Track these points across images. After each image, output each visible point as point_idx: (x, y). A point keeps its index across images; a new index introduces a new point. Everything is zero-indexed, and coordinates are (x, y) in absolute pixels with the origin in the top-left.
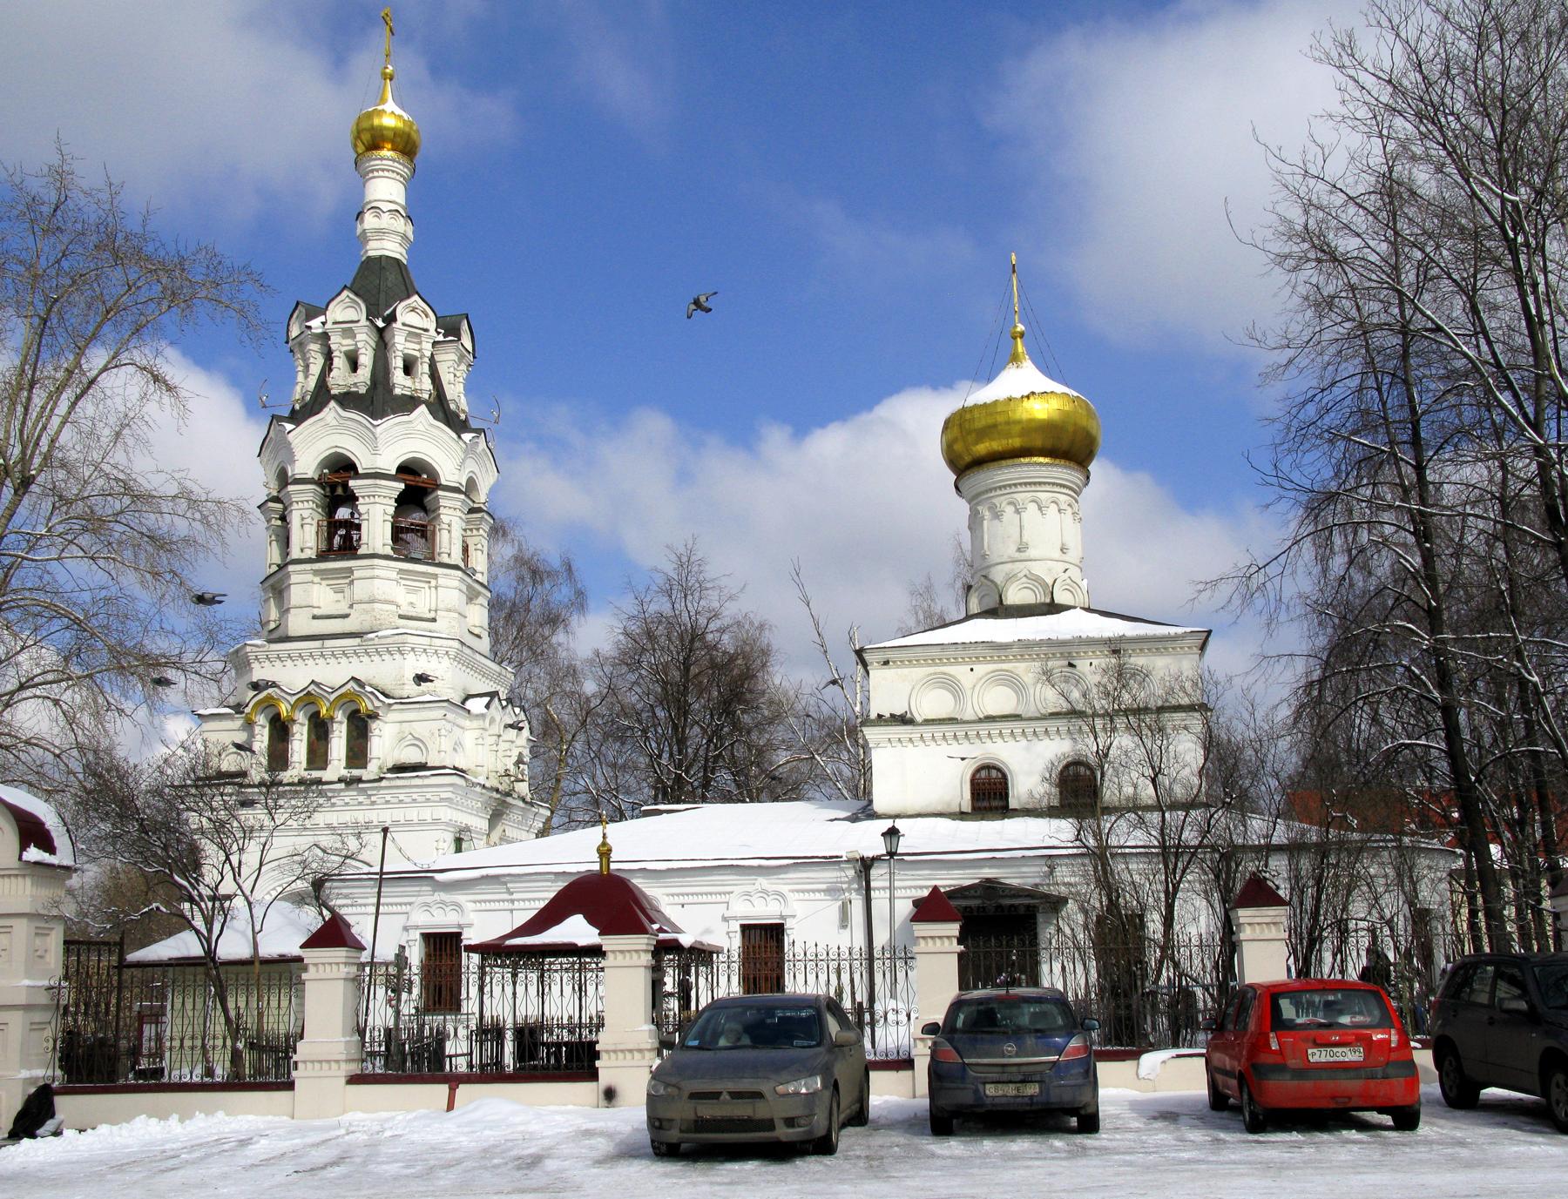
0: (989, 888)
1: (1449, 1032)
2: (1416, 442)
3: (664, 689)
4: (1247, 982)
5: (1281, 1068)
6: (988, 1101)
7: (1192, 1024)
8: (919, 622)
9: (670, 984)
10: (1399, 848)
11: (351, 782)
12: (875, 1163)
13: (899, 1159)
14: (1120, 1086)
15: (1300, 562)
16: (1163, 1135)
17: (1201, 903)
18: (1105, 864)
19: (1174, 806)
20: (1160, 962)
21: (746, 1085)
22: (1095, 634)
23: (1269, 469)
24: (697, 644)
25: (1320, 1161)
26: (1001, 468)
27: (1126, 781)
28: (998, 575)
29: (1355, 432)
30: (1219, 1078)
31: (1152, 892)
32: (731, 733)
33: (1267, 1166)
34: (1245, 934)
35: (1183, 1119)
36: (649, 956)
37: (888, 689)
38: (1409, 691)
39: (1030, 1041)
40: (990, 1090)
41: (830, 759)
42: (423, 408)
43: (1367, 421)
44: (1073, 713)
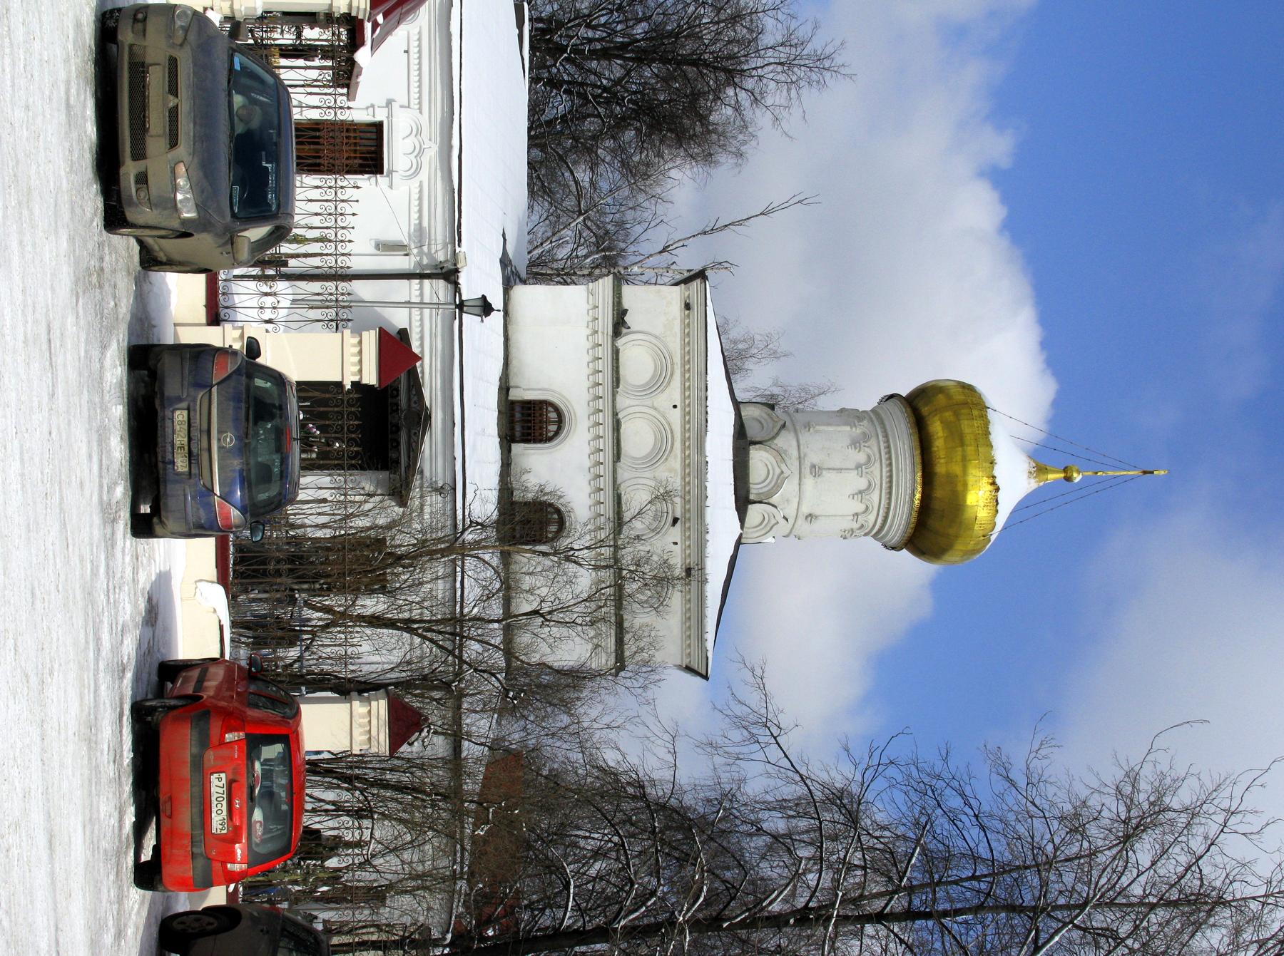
0: (421, 418)
1: (244, 923)
2: (910, 915)
3: (670, 34)
4: (304, 708)
5: (204, 743)
6: (168, 413)
7: (259, 643)
8: (735, 342)
9: (312, 34)
10: (454, 877)
12: (94, 279)
13: (100, 305)
14: (189, 562)
15: (780, 783)
16: (130, 609)
17: (396, 657)
18: (444, 553)
19: (508, 632)
20: (328, 610)
21: (186, 127)
22: (710, 549)
23: (891, 753)
24: (722, 76)
25: (98, 783)
26: (912, 448)
27: (538, 578)
28: (785, 441)
29: (923, 850)
30: (195, 673)
31: (410, 605)
32: (612, 115)
33: (92, 726)
34: (359, 707)
35: (149, 631)
36: (344, 10)
37: (656, 306)
38: (628, 893)
39: (236, 463)
40: (180, 416)
41: (577, 234)
43: (937, 861)
44: (619, 522)
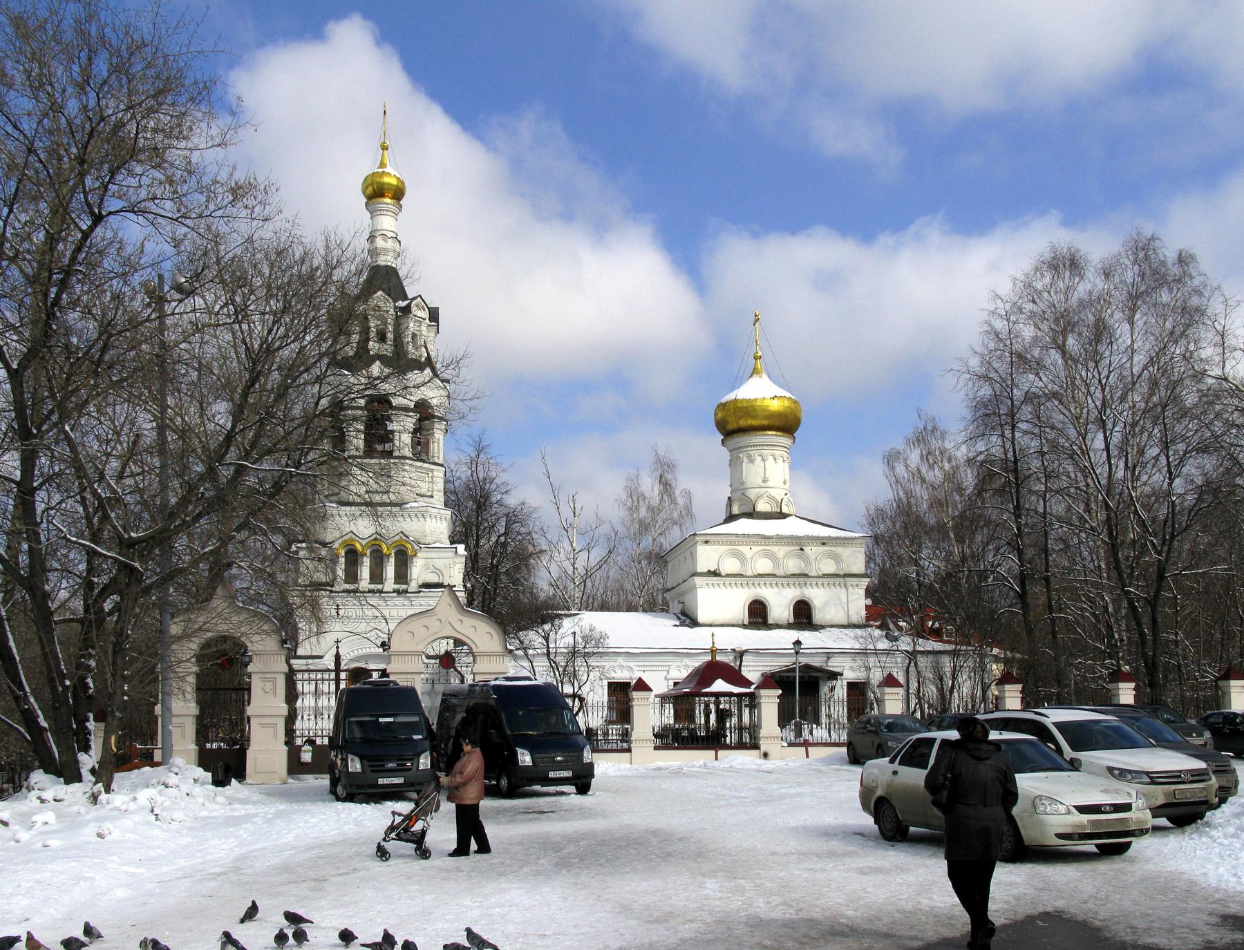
22: (815, 534)
28: (752, 494)
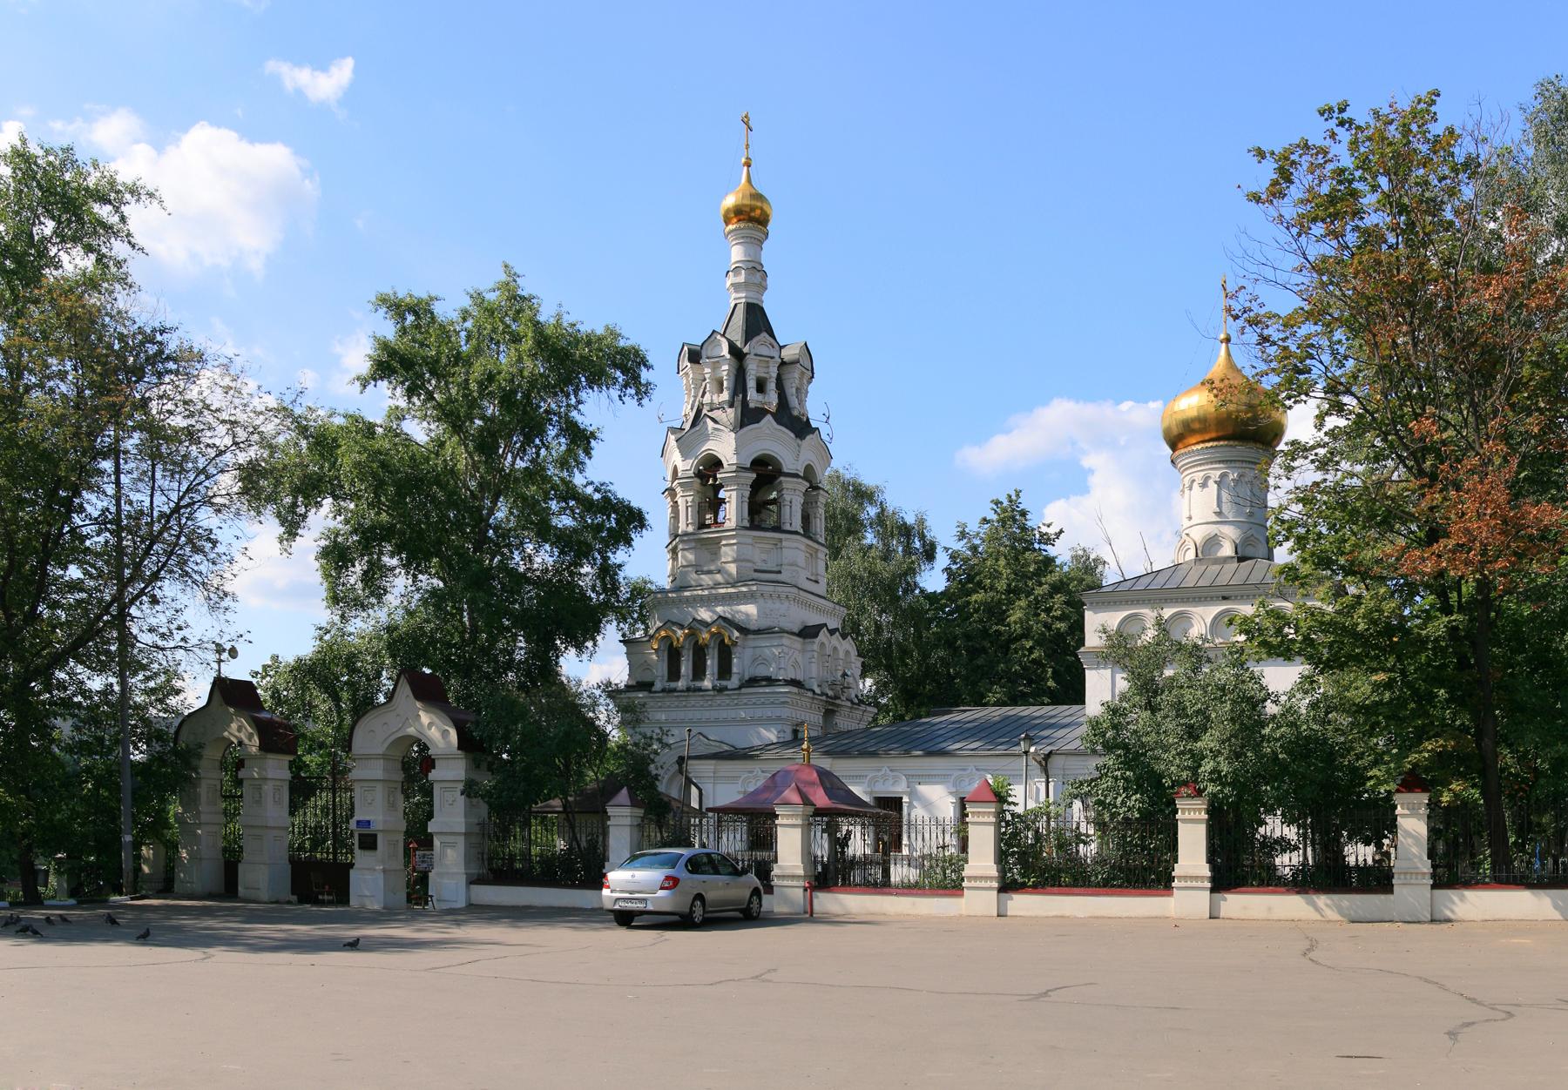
11: (721, 690)
42: (769, 417)
